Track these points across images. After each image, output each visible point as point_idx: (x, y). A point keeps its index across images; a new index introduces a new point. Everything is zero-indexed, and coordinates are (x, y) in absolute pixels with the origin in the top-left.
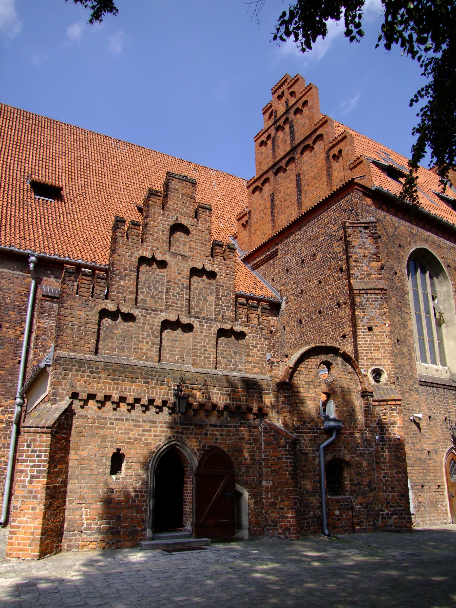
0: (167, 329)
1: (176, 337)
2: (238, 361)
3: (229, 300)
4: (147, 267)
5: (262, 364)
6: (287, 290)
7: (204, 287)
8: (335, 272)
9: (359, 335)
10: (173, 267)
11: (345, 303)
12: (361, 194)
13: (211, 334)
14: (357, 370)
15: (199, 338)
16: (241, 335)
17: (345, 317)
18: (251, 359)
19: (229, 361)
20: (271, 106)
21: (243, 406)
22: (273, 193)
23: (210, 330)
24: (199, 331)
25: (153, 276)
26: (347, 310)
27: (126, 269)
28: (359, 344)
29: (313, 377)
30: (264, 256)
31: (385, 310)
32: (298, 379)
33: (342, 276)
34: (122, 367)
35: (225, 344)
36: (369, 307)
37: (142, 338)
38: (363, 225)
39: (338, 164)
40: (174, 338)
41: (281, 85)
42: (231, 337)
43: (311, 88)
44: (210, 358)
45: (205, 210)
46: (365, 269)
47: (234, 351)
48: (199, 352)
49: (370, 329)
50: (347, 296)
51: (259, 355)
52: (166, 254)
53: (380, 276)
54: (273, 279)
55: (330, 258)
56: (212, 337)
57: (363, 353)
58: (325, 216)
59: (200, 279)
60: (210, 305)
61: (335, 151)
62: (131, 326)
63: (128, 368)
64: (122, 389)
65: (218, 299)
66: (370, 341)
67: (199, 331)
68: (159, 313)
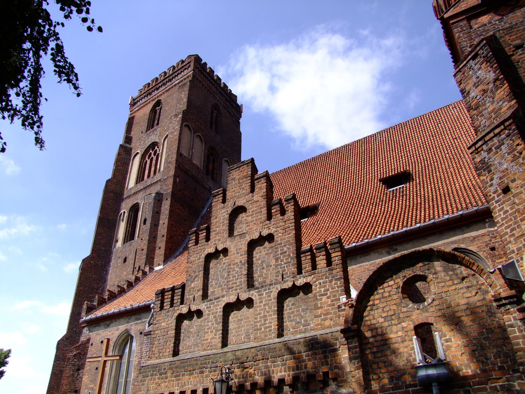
2: (309, 319)
3: (289, 255)
4: (216, 261)
10: (232, 250)
16: (307, 288)
19: (298, 323)
21: (302, 375)
23: (270, 296)
27: (195, 272)
29: (394, 307)
32: (371, 317)
34: (182, 363)
35: (292, 305)
37: (208, 329)
38: (470, 57)
40: (239, 318)
42: (298, 294)
45: (259, 180)
48: (259, 324)
51: (329, 303)
52: (226, 241)
57: (506, 233)
59: (261, 247)
63: (187, 362)
64: (182, 383)
66: (511, 209)
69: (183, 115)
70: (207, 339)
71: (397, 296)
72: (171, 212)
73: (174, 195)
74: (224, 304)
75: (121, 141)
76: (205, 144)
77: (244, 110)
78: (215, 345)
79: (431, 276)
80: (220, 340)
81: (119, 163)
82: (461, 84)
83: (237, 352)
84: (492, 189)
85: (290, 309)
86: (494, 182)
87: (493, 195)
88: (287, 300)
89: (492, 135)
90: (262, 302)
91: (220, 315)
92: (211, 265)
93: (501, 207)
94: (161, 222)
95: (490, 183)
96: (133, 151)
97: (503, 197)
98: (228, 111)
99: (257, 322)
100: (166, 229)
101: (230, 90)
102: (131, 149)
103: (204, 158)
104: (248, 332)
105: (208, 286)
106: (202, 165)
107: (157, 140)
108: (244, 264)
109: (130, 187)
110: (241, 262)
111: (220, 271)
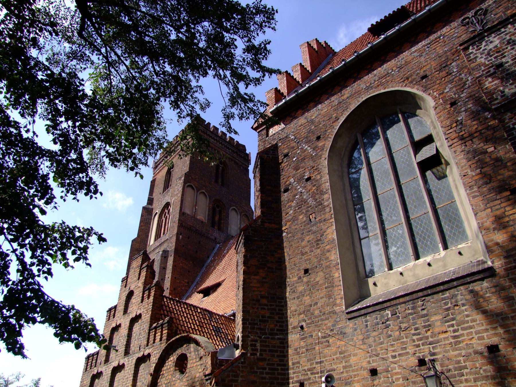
69: (185, 177)
72: (174, 266)
73: (177, 251)
75: (145, 203)
76: (209, 198)
81: (142, 224)
94: (166, 276)
96: (154, 210)
98: (235, 162)
100: (170, 282)
102: (153, 209)
103: (209, 211)
106: (207, 218)
107: (169, 201)
109: (151, 244)
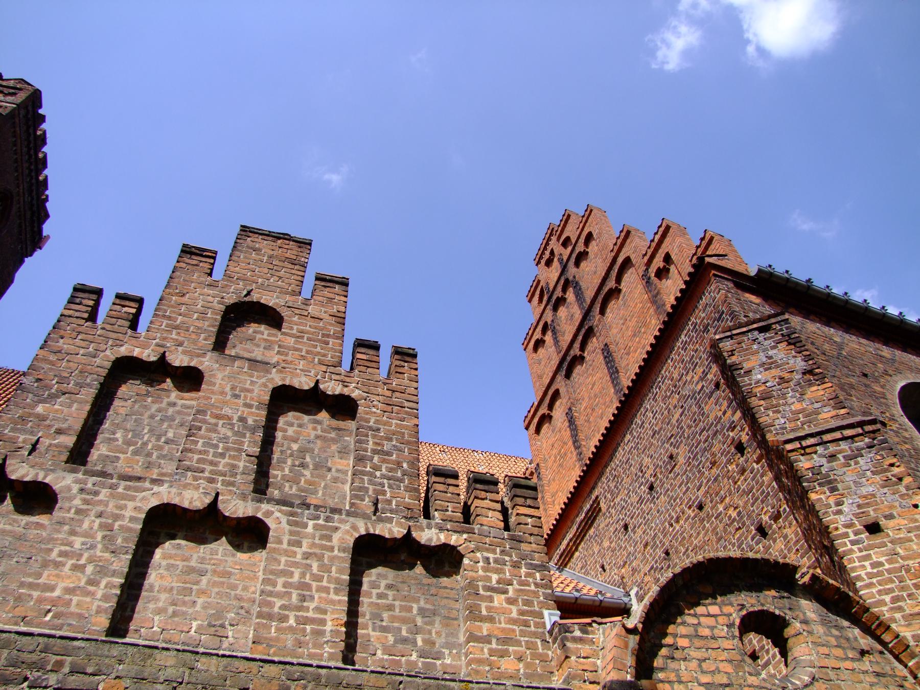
0: (173, 538)
1: (202, 560)
2: (440, 641)
3: (399, 464)
4: (143, 387)
5: (530, 646)
6: (634, 570)
7: (317, 437)
8: (729, 462)
9: (846, 553)
10: (218, 381)
11: (776, 517)
12: (731, 285)
13: (332, 549)
14: (887, 637)
15: (283, 559)
16: (444, 560)
17: (789, 551)
18: (485, 628)
19: (405, 641)
20: (539, 282)
22: (570, 409)
23: (329, 538)
24: (285, 539)
25: (155, 407)
26: (787, 531)
28: (859, 578)
29: (729, 668)
30: (575, 527)
31: (896, 470)
32: (672, 677)
33: (746, 461)
35: (389, 587)
36: (847, 476)
38: (755, 326)
39: (669, 282)
40: (193, 563)
41: (547, 244)
42: (412, 567)
43: (591, 211)
44: (323, 622)
46: (797, 406)
47: (422, 611)
48: (279, 603)
49: (874, 528)
50: (775, 495)
51: (514, 615)
53: (843, 411)
54: (603, 567)
55: (706, 441)
56: (332, 559)
58: (671, 369)
60: (335, 480)
61: (658, 262)
62: (39, 525)
65: (360, 459)
67: (285, 539)
68: (147, 484)
70: (52, 589)
71: (730, 642)
74: (154, 502)
77: (47, 247)
78: (80, 616)
79: (798, 625)
80: (112, 604)
82: (733, 355)
83: (204, 659)
84: (842, 519)
85: (380, 596)
86: (845, 508)
87: (842, 530)
88: (374, 571)
89: (837, 435)
90: (299, 544)
91: (130, 530)
92: (123, 390)
93: (864, 553)
95: (834, 508)
97: (867, 537)
99: (271, 594)
101: (47, 196)
104: (219, 614)
105: (94, 437)
108: (253, 430)
110: (242, 419)
111: (152, 417)
